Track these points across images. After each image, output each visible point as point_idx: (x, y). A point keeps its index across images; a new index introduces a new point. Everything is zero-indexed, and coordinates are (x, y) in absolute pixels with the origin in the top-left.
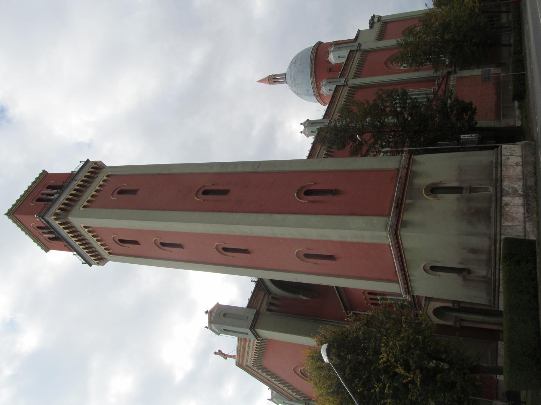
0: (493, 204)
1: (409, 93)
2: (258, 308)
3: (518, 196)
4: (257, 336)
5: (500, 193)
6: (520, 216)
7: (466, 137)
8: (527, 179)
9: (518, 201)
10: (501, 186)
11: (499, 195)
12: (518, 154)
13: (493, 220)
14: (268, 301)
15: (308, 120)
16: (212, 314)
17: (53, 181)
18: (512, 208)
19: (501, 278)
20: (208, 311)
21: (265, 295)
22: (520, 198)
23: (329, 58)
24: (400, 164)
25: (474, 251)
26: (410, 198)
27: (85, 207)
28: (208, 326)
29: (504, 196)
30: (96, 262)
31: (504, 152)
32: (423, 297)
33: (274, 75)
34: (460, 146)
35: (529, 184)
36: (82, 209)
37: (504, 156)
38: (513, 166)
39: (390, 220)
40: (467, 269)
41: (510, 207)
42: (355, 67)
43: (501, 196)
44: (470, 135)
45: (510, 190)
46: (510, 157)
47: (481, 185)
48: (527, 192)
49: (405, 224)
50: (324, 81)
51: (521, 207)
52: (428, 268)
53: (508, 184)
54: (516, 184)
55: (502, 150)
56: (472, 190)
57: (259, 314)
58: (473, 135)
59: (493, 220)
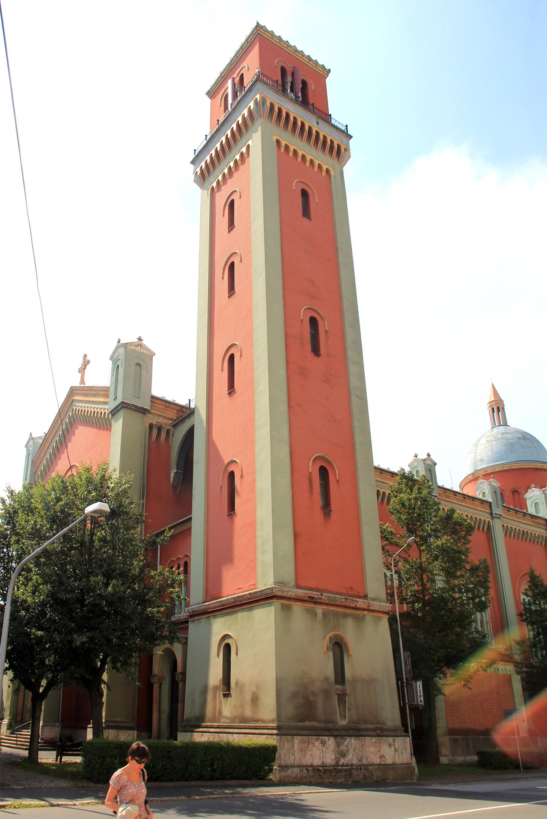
0: (322, 725)
2: (152, 411)
3: (336, 758)
4: (114, 412)
6: (307, 761)
7: (418, 689)
9: (329, 758)
10: (351, 736)
12: (397, 759)
13: (300, 724)
14: (164, 425)
15: (436, 464)
16: (137, 347)
17: (313, 89)
18: (318, 749)
20: (142, 340)
21: (171, 419)
22: (334, 760)
23: (534, 489)
25: (255, 700)
26: (324, 615)
27: (278, 142)
28: (121, 342)
29: (335, 739)
30: (198, 170)
32: (187, 634)
33: (503, 408)
36: (275, 138)
37: (394, 740)
38: (379, 751)
41: (320, 748)
42: (536, 532)
43: (335, 736)
44: (422, 694)
45: (345, 748)
46: (393, 748)
47: (349, 709)
49: (286, 609)
50: (496, 484)
51: (321, 761)
53: (353, 745)
56: (342, 697)
57: (145, 414)
58: (422, 698)
59: (300, 724)
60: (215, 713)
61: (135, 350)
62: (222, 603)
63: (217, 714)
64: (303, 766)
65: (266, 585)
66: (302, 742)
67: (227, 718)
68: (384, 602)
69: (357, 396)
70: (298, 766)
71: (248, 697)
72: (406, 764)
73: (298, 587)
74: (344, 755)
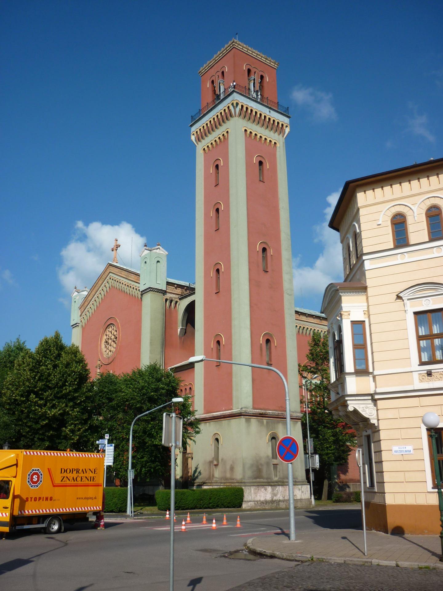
0: (265, 480)
1: (290, 465)
2: (167, 291)
3: (272, 497)
5: (273, 484)
8: (284, 503)
9: (268, 497)
10: (279, 485)
11: (272, 484)
13: (254, 480)
14: (174, 299)
17: (268, 81)
18: (263, 493)
19: (214, 487)
24: (293, 412)
25: (232, 469)
26: (267, 423)
27: (246, 130)
31: (304, 487)
34: (310, 454)
35: (281, 503)
39: (251, 410)
40: (218, 463)
41: (264, 492)
43: (271, 486)
44: (318, 462)
45: (276, 492)
46: (301, 491)
47: (279, 472)
48: (275, 502)
49: (248, 421)
52: (217, 437)
53: (281, 490)
54: (280, 495)
55: (306, 486)
58: (318, 464)
59: (254, 480)
60: (210, 475)
61: (156, 252)
62: (213, 416)
63: (212, 475)
64: (255, 501)
65: (238, 409)
66: (255, 489)
67: (217, 478)
68: (299, 413)
69: (288, 294)
70: (253, 501)
71: (228, 467)
72: (308, 499)
73: (254, 408)
74: (276, 495)
